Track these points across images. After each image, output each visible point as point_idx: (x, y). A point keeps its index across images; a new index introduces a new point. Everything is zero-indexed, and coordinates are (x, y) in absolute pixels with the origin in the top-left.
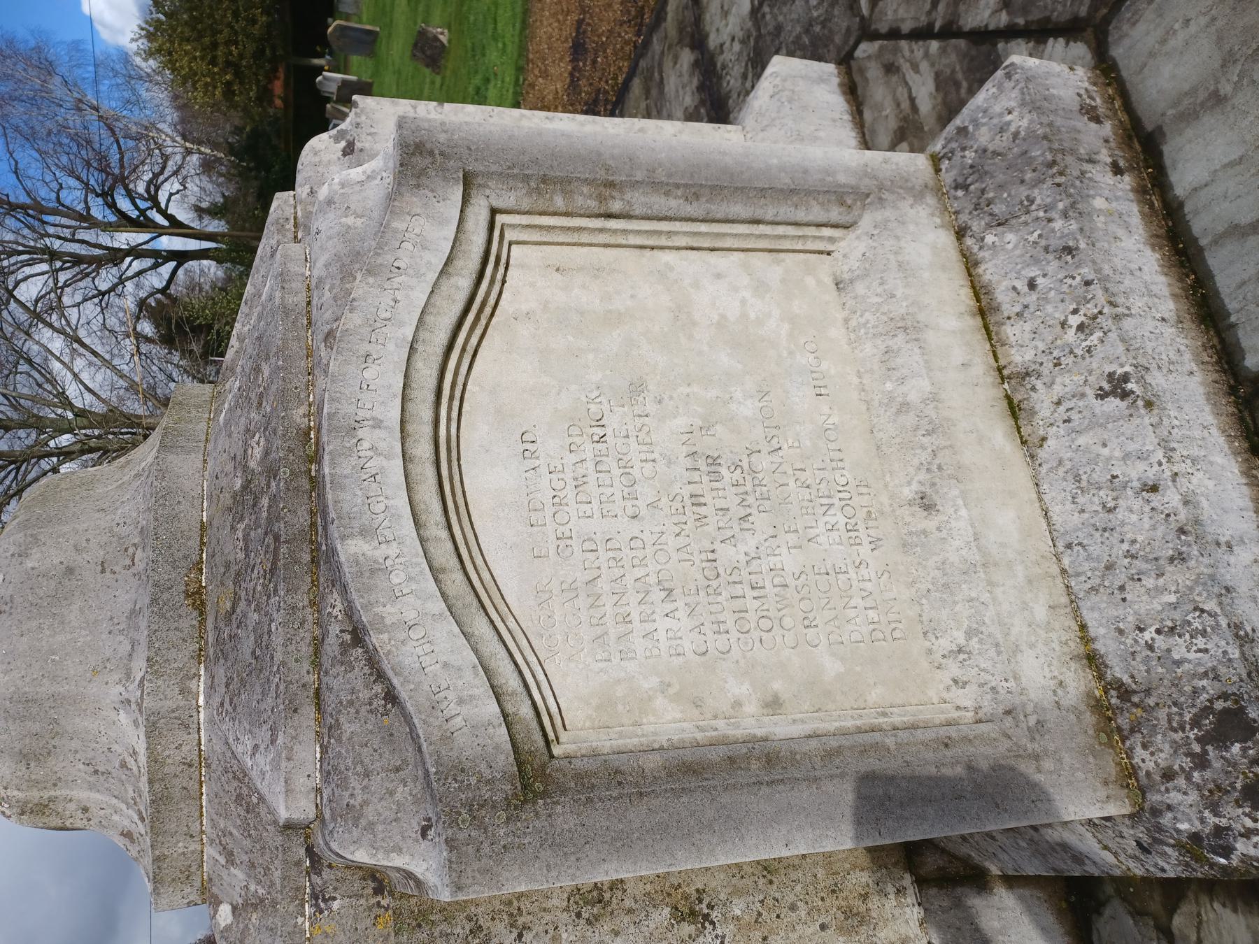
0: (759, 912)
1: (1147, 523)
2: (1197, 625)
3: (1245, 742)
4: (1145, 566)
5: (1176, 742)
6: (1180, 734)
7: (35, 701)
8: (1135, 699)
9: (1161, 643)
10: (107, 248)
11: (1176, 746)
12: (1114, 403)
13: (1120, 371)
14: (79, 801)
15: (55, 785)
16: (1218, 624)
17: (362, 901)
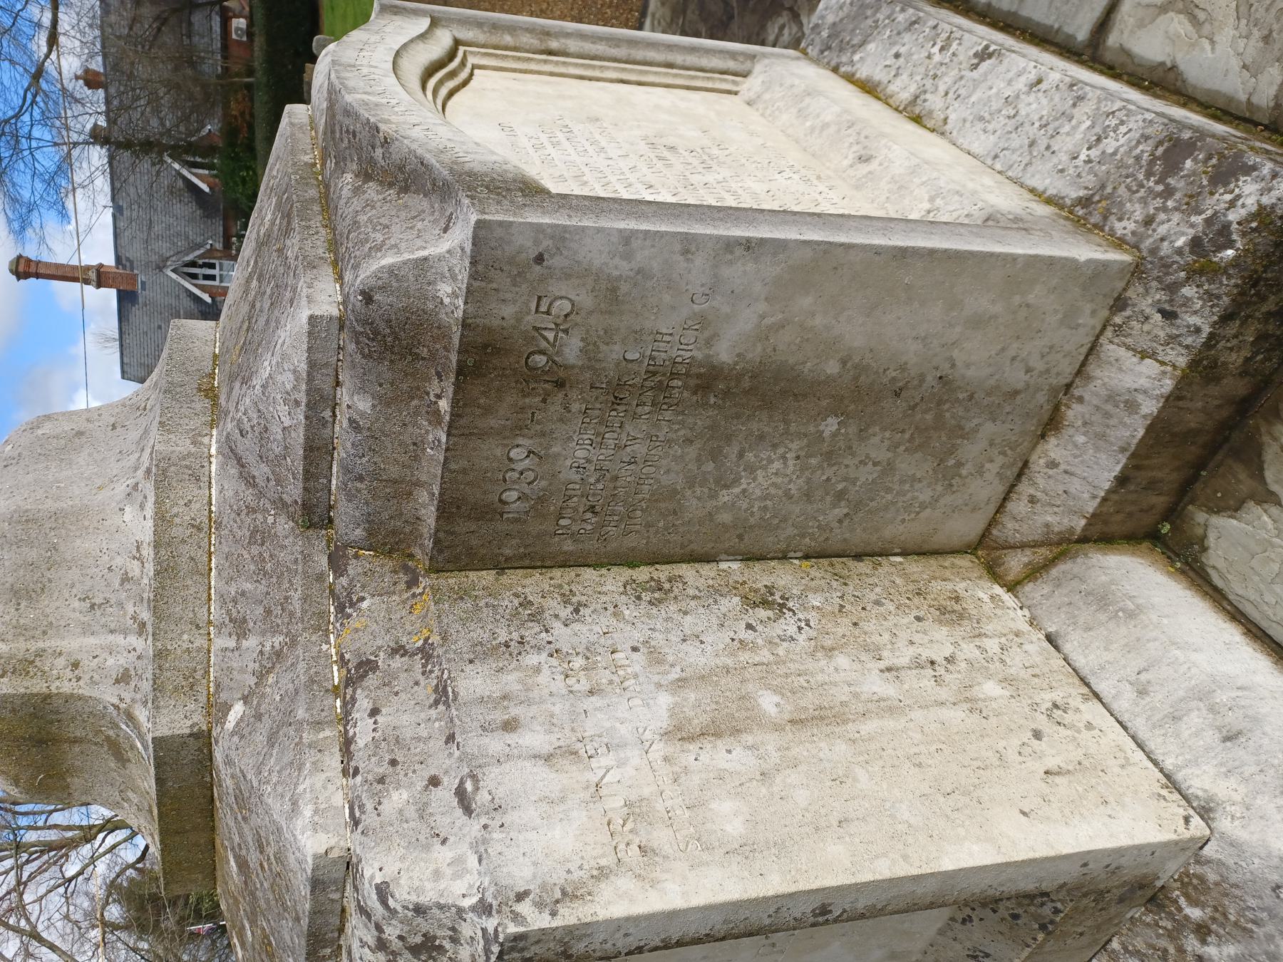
0: (841, 605)
1: (1044, 101)
2: (1114, 122)
3: (1192, 154)
4: (1057, 124)
5: (1142, 198)
6: (1143, 190)
7: (35, 521)
8: (1097, 198)
9: (1094, 153)
10: (81, 828)
11: (1143, 201)
12: (986, 65)
13: (980, 48)
14: (69, 654)
15: (45, 633)
16: (1129, 110)
17: (395, 597)
